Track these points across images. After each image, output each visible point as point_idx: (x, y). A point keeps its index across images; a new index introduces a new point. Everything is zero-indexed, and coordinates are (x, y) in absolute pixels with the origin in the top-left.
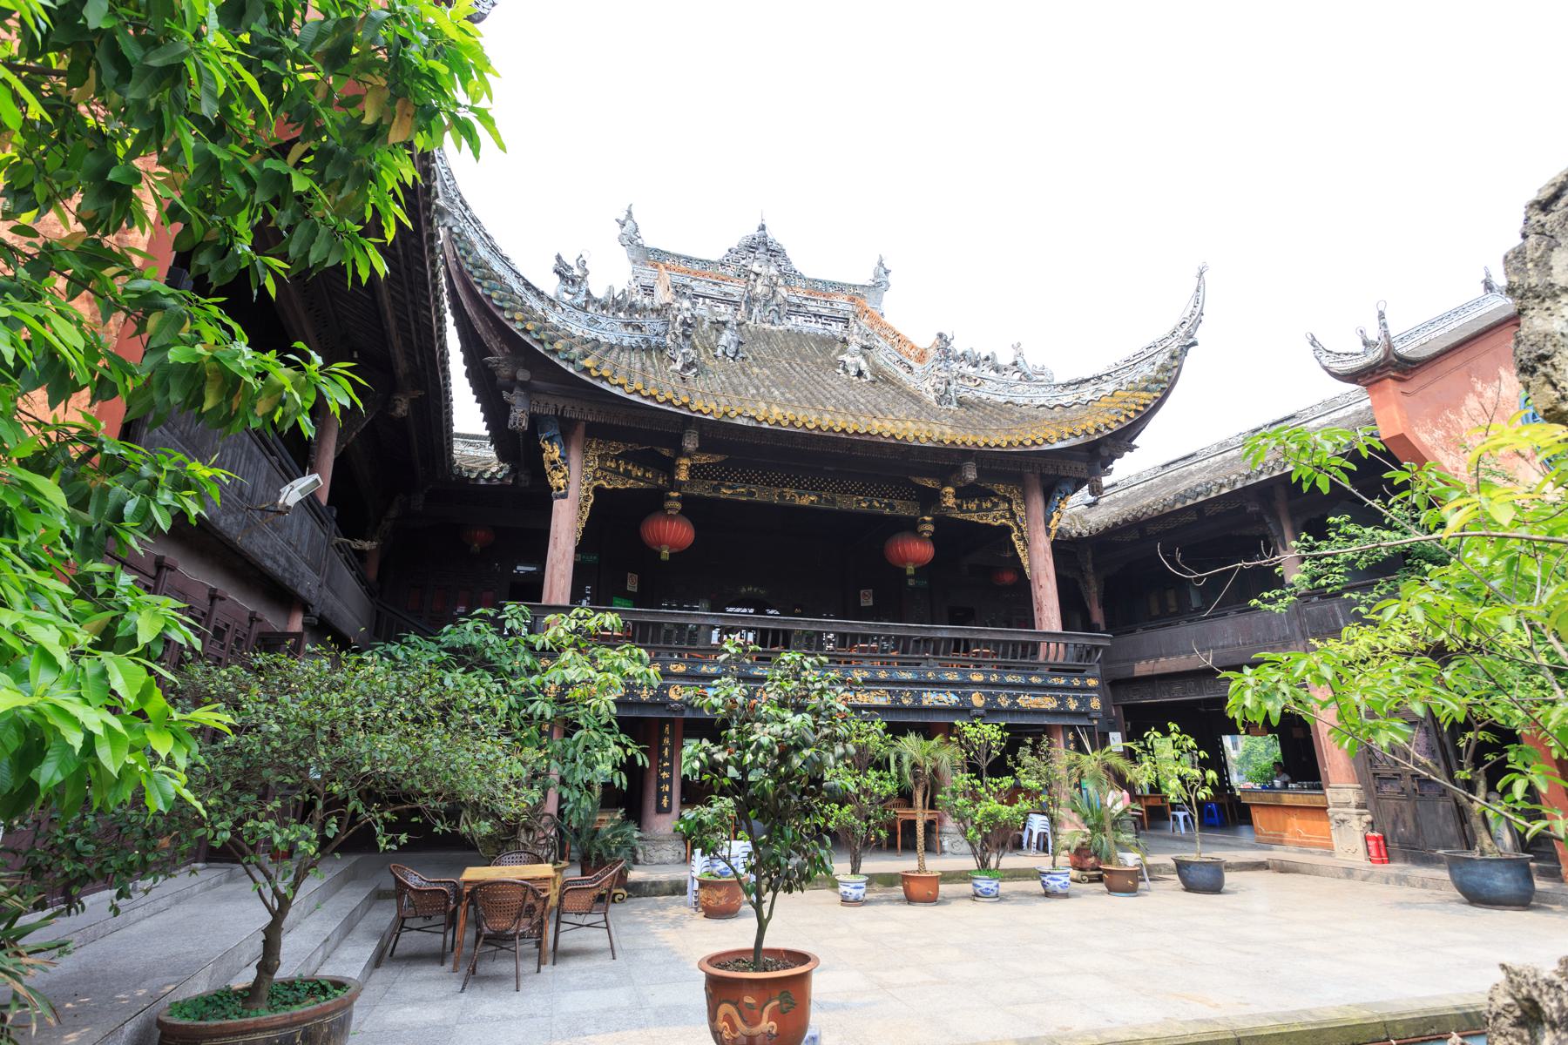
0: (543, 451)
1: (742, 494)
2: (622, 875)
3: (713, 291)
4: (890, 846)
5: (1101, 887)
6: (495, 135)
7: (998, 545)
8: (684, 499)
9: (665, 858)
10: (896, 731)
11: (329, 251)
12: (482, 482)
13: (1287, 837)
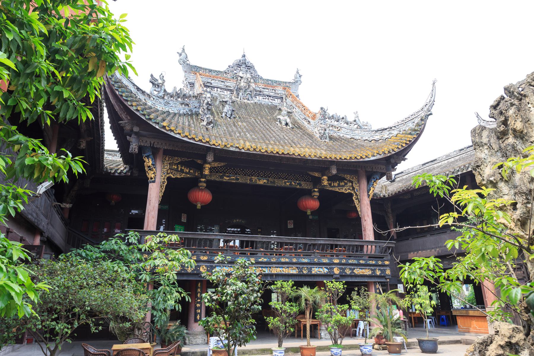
0: (145, 161)
1: (233, 179)
2: (179, 348)
3: (221, 85)
4: (292, 336)
5: (386, 352)
6: (133, 68)
7: (348, 199)
8: (207, 182)
9: (198, 342)
10: (298, 285)
11: (73, 113)
12: (117, 174)
13: (471, 329)
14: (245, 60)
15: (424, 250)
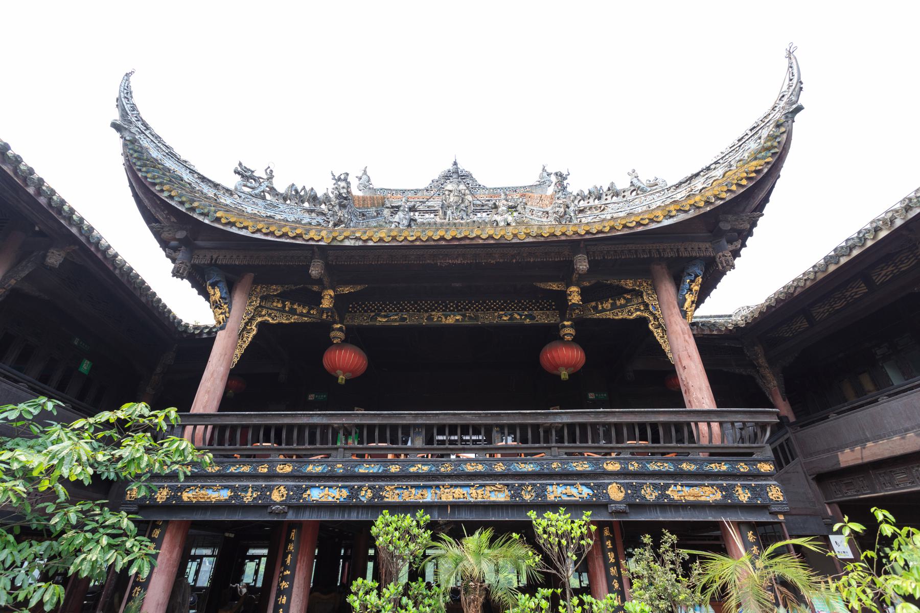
1: (395, 320)
12: (205, 336)
14: (457, 168)
15: (881, 438)
